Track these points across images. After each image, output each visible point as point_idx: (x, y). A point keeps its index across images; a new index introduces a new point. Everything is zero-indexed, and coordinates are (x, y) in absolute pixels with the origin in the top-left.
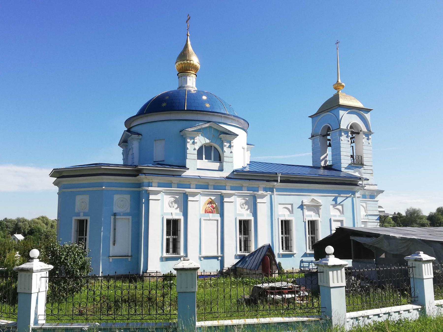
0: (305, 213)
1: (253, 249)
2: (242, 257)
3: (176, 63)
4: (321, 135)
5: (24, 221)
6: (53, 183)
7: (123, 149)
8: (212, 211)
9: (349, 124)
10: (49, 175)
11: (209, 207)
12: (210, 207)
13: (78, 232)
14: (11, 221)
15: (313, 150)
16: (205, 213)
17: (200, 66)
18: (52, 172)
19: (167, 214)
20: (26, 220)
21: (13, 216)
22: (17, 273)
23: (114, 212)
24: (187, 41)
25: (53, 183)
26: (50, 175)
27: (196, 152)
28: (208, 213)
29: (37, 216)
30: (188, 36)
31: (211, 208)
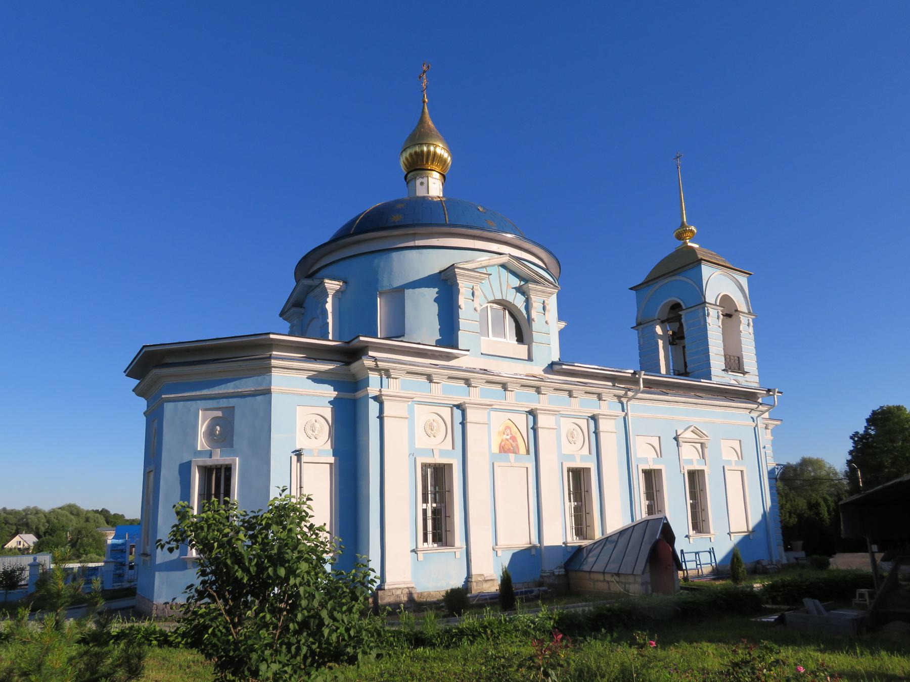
0: (682, 456)
1: (598, 535)
2: (570, 555)
3: (405, 150)
4: (659, 319)
5: (37, 512)
6: (133, 391)
7: (290, 325)
8: (514, 449)
9: (719, 294)
10: (125, 372)
11: (507, 440)
12: (510, 440)
13: (206, 495)
14: (14, 513)
15: (640, 348)
16: (500, 452)
17: (452, 159)
18: (132, 362)
19: (423, 451)
20: (40, 511)
21: (17, 504)
22: (880, 478)
23: (298, 448)
24: (423, 112)
25: (133, 391)
26: (127, 373)
27: (476, 316)
28: (505, 452)
29: (60, 505)
30: (424, 102)
31: (511, 441)
